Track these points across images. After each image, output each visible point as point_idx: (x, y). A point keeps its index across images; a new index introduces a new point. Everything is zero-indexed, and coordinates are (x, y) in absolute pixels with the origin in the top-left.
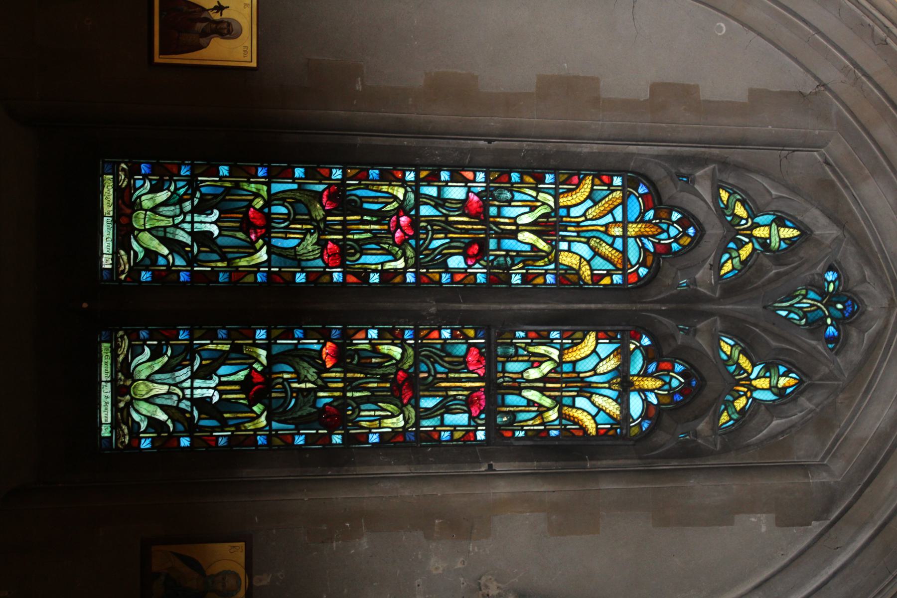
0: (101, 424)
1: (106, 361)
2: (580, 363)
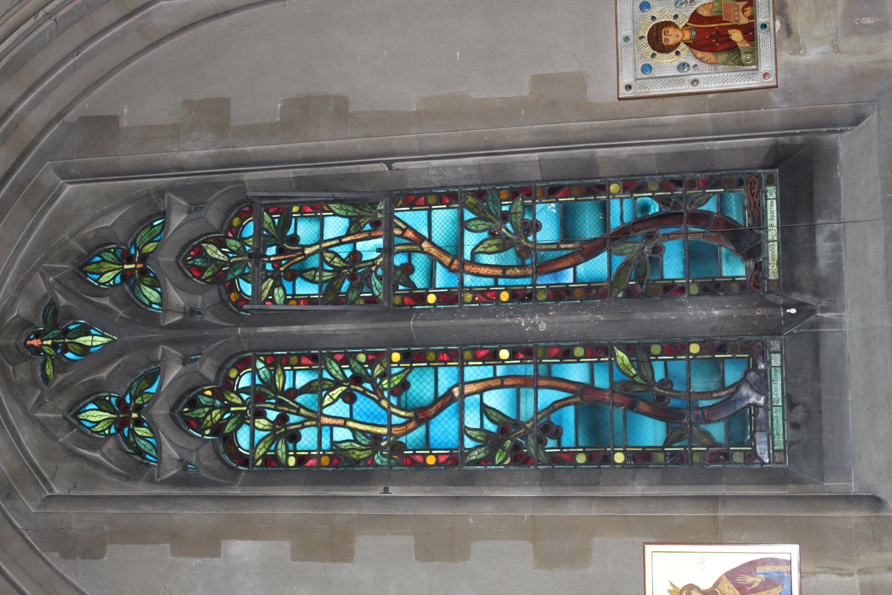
1: (773, 262)
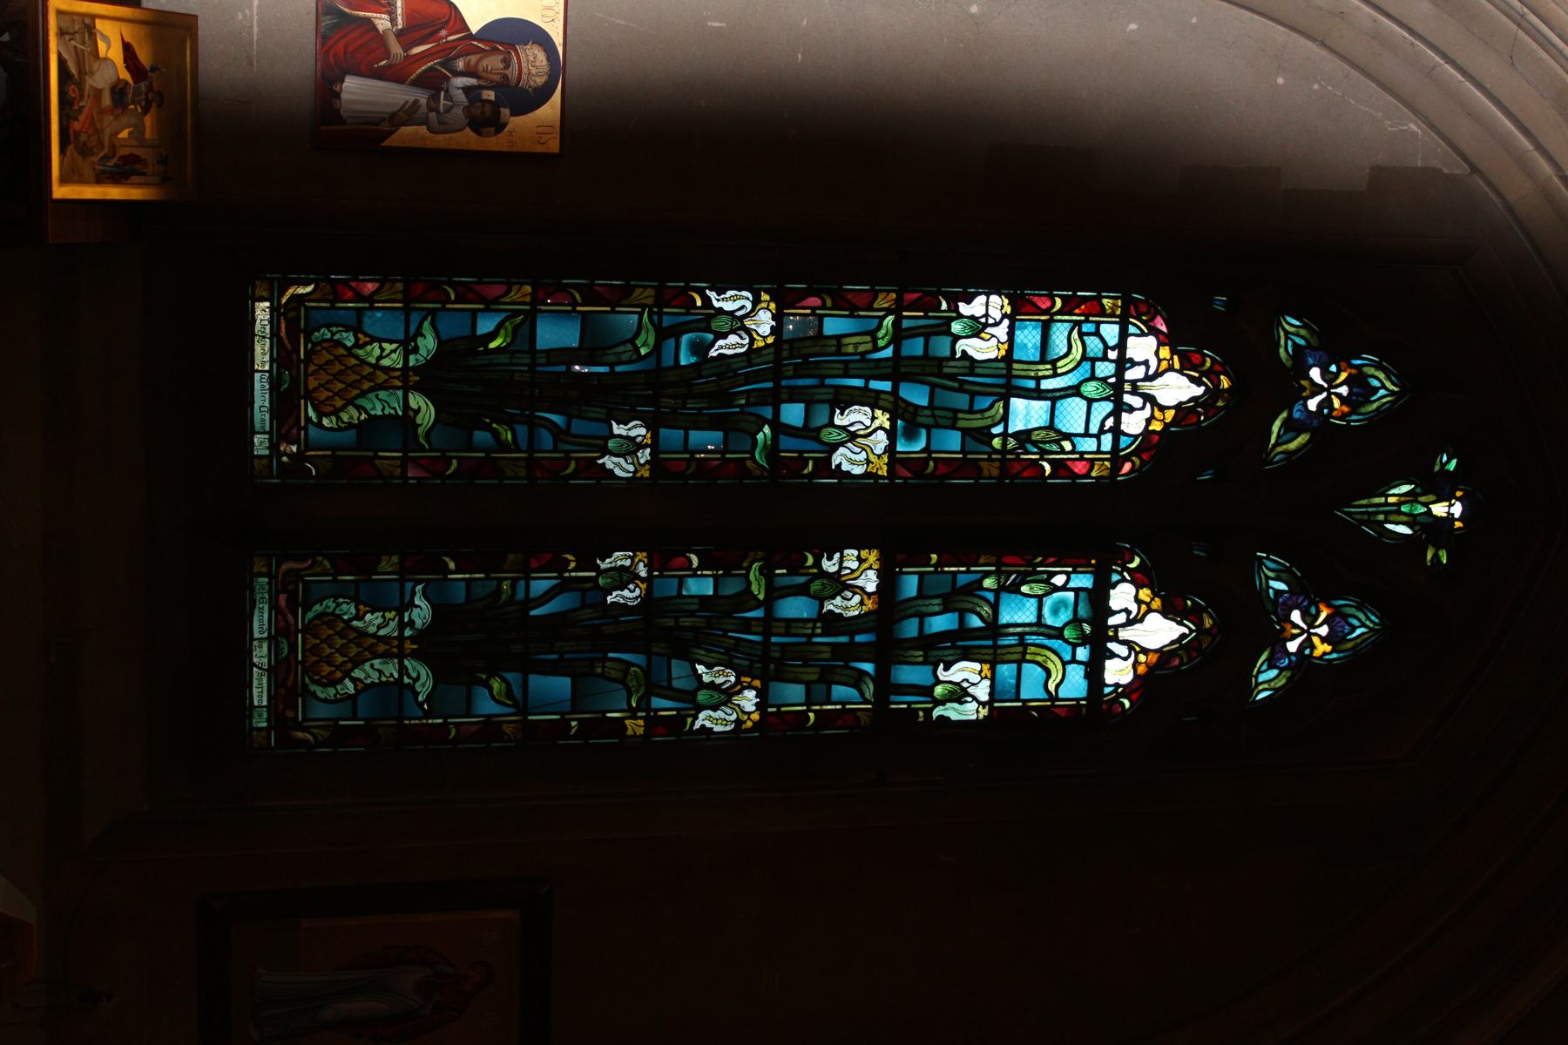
1: (261, 606)
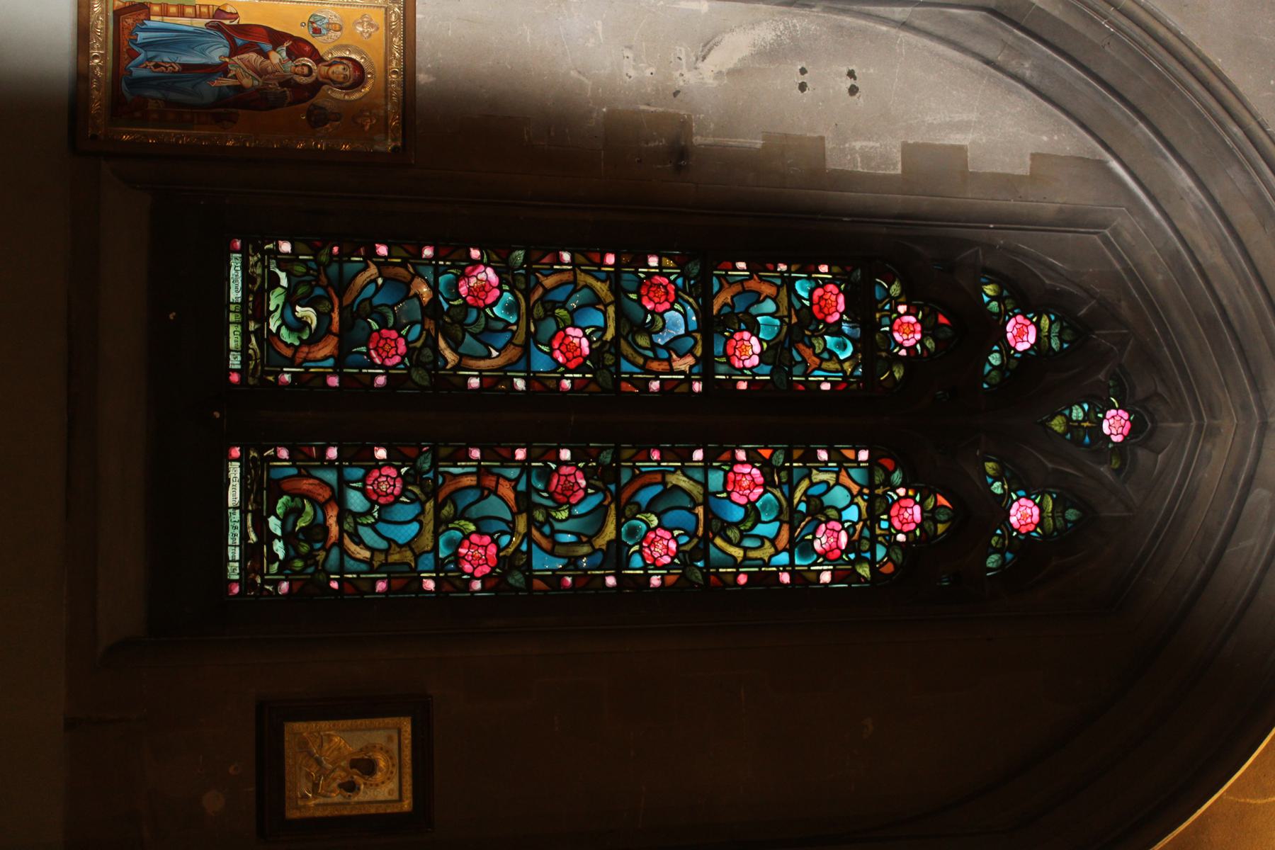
0: (229, 351)
1: (234, 483)
2: (476, 498)
